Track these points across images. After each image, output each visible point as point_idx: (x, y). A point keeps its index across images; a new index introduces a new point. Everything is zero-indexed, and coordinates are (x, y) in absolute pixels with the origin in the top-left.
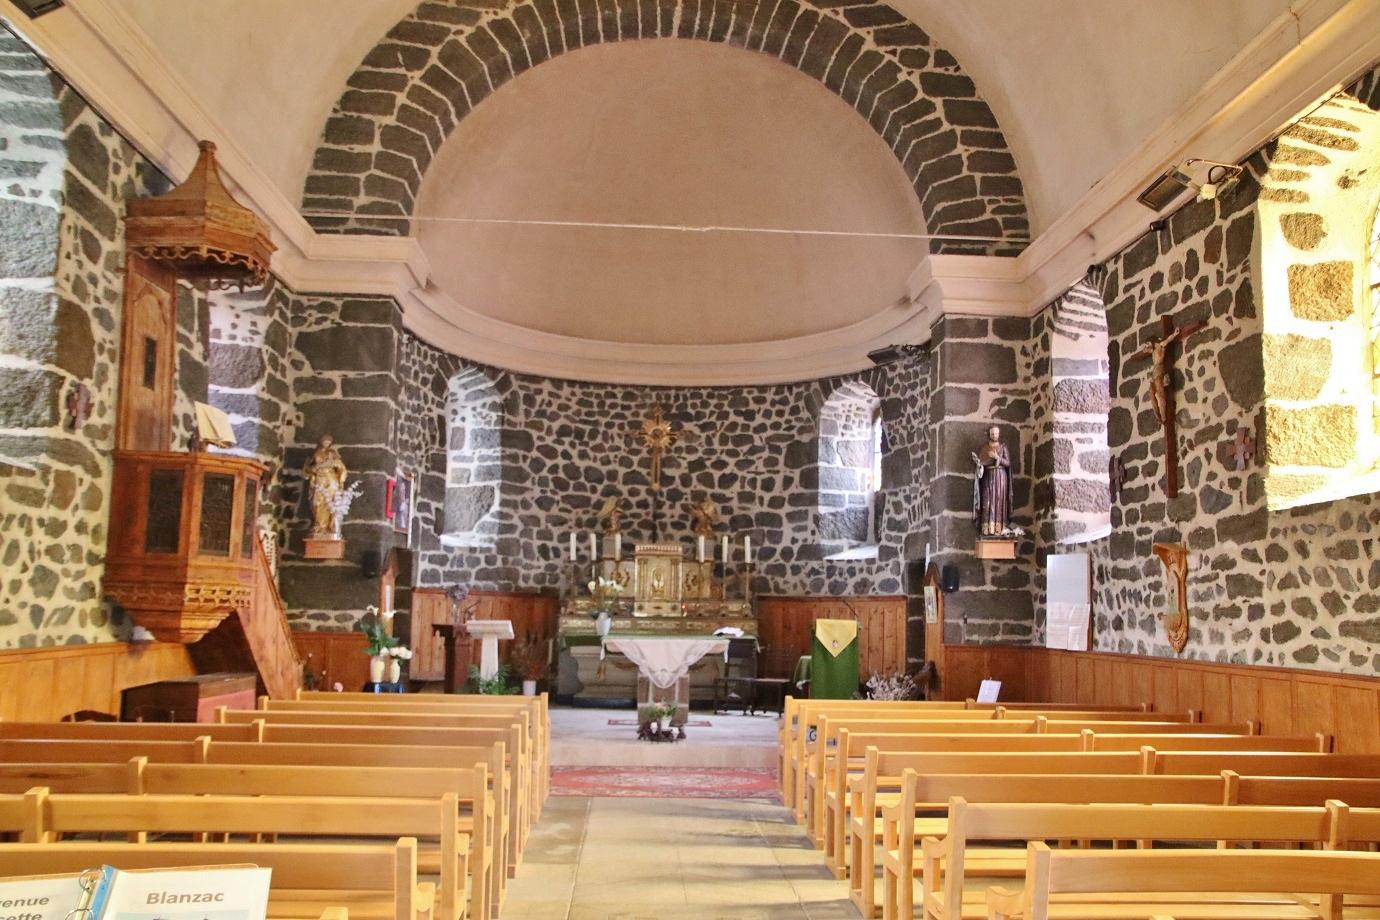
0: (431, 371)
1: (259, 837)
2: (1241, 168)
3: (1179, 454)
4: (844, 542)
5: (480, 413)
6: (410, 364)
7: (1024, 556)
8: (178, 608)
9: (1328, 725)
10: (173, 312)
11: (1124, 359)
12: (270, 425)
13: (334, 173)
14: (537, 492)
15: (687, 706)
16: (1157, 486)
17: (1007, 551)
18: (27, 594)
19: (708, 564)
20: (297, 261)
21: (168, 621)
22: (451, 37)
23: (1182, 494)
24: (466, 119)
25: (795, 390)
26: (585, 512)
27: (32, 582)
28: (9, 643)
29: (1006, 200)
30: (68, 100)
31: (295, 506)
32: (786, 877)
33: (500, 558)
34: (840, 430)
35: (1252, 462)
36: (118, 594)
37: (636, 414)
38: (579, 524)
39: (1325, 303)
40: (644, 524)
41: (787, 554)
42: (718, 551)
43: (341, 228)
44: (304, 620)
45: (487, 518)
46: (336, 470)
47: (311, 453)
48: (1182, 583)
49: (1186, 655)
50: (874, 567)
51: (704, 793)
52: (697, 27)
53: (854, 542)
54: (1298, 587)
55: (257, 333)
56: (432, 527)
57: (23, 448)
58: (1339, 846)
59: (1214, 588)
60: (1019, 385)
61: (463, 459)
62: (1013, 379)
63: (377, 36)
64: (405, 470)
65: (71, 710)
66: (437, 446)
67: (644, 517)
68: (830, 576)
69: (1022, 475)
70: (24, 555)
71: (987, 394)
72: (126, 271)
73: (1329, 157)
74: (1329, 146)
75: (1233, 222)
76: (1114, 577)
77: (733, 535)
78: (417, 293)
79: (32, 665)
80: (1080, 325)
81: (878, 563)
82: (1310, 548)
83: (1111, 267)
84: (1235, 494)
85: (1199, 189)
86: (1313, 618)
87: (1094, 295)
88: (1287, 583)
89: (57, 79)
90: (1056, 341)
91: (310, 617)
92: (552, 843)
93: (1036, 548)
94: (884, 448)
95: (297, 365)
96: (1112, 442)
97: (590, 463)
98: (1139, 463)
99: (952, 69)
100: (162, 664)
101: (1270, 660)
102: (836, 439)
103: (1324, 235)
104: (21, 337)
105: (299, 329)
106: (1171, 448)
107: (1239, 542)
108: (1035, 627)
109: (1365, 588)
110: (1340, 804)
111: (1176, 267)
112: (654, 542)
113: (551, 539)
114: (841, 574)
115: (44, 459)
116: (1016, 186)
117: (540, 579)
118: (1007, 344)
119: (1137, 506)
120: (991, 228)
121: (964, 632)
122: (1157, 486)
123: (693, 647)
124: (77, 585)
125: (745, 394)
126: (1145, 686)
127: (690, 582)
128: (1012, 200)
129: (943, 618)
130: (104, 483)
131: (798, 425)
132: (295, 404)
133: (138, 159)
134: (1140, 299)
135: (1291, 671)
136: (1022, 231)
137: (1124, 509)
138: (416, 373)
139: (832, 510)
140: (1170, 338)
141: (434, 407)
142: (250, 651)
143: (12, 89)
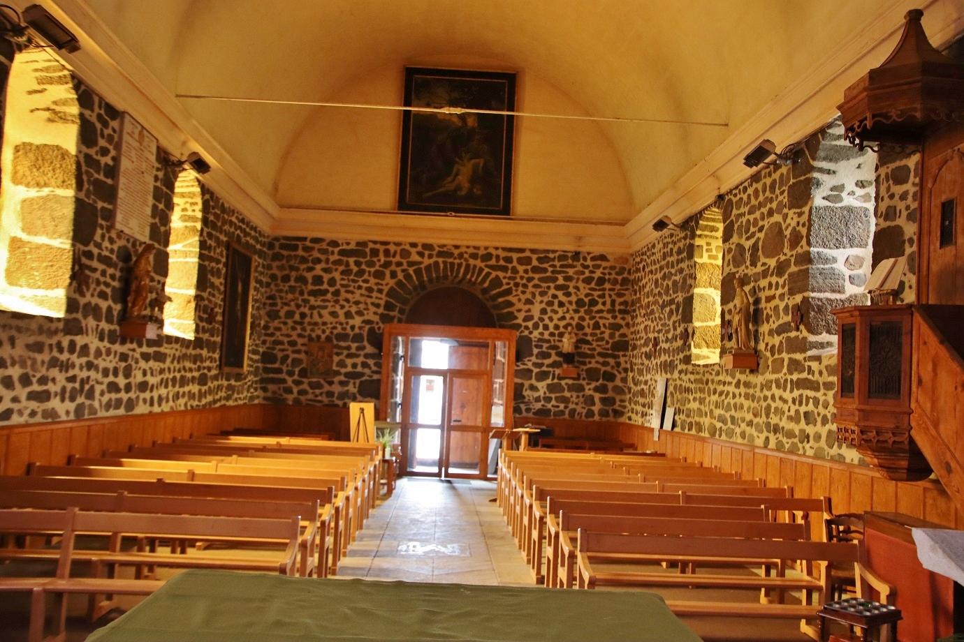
28: (852, 460)
82: (17, 342)
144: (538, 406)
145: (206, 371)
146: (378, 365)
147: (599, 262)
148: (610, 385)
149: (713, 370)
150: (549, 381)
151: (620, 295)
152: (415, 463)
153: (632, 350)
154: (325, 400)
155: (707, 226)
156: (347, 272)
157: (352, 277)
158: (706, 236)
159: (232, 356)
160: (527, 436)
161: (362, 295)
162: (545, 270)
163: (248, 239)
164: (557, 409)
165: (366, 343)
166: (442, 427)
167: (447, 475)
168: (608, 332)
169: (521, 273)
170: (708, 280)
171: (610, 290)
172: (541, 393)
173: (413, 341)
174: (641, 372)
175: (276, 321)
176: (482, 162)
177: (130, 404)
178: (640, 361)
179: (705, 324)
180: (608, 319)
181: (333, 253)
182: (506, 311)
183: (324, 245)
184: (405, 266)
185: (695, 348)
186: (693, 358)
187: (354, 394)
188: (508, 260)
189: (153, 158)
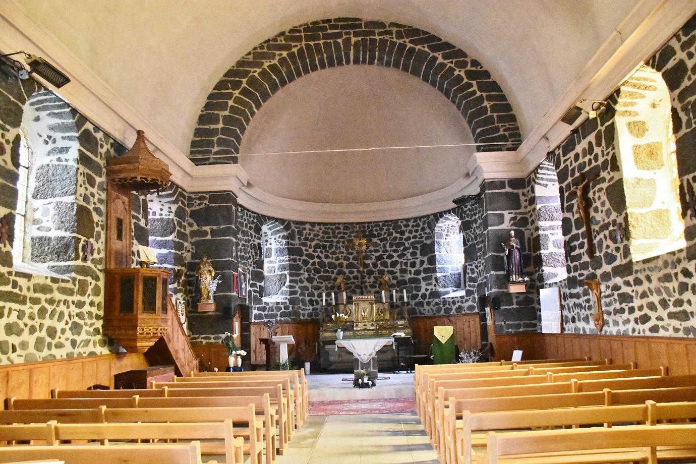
0: (253, 223)
1: (168, 440)
2: (606, 103)
3: (593, 237)
4: (450, 289)
5: (278, 241)
6: (243, 221)
7: (531, 290)
8: (135, 337)
9: (665, 362)
10: (129, 206)
11: (566, 194)
12: (180, 253)
13: (203, 138)
14: (306, 275)
15: (377, 370)
16: (585, 254)
17: (521, 289)
18: (68, 334)
19: (387, 304)
20: (188, 179)
21: (131, 344)
22: (251, 74)
23: (596, 256)
24: (261, 109)
25: (422, 220)
26: (329, 283)
27: (70, 329)
28: (61, 356)
29: (509, 125)
30: (79, 118)
31: (193, 289)
32: (409, 450)
33: (291, 306)
34: (445, 237)
35: (624, 239)
36: (110, 332)
37: (350, 236)
38: (327, 288)
39: (651, 162)
40: (357, 287)
41: (424, 296)
42: (391, 297)
43: (207, 162)
44: (200, 340)
45: (284, 288)
46: (210, 271)
47: (198, 264)
48: (599, 299)
49: (603, 333)
50: (464, 300)
51: (381, 412)
52: (361, 59)
53: (455, 289)
54: (648, 297)
55: (171, 212)
56: (258, 294)
57: (65, 271)
58: (653, 423)
59: (613, 300)
60: (522, 210)
61: (272, 262)
62: (519, 207)
63: (219, 76)
64: (243, 269)
65: (91, 385)
66: (258, 257)
67: (357, 283)
68: (444, 306)
69: (527, 252)
70: (66, 317)
71: (507, 215)
72: (107, 190)
73: (645, 95)
74: (644, 89)
75: (606, 127)
76: (570, 297)
77: (398, 289)
78: (244, 188)
79: (72, 366)
80: (547, 180)
81: (466, 298)
82: (652, 278)
83: (557, 152)
84: (618, 255)
85: (588, 113)
86: (656, 311)
87: (550, 165)
88: (644, 295)
89: (74, 111)
90: (537, 187)
91: (202, 338)
92: (305, 438)
93: (536, 284)
94: (465, 244)
95: (191, 225)
96: (564, 234)
97: (330, 260)
98: (576, 243)
99: (479, 67)
100: (132, 363)
101: (639, 333)
102: (442, 241)
103: (647, 130)
104: (62, 222)
105: (191, 209)
106: (589, 235)
107: (622, 277)
108: (538, 324)
109: (677, 296)
110: (652, 402)
111: (584, 150)
112: (362, 295)
113: (314, 296)
114: (449, 304)
115: (73, 275)
116: (513, 118)
117: (310, 315)
118: (515, 191)
119: (577, 263)
120: (503, 138)
121: (504, 328)
122: (585, 254)
123: (377, 343)
124: (91, 329)
125: (399, 223)
126: (587, 349)
127: (379, 312)
128: (512, 125)
129: (494, 322)
130: (101, 284)
131: (425, 236)
132: (191, 243)
133: (111, 141)
134: (571, 166)
135: (648, 338)
136: (518, 139)
137: (572, 265)
138: (246, 224)
139: (443, 274)
140: (584, 183)
141: (256, 239)
142: (171, 355)
143: (57, 118)
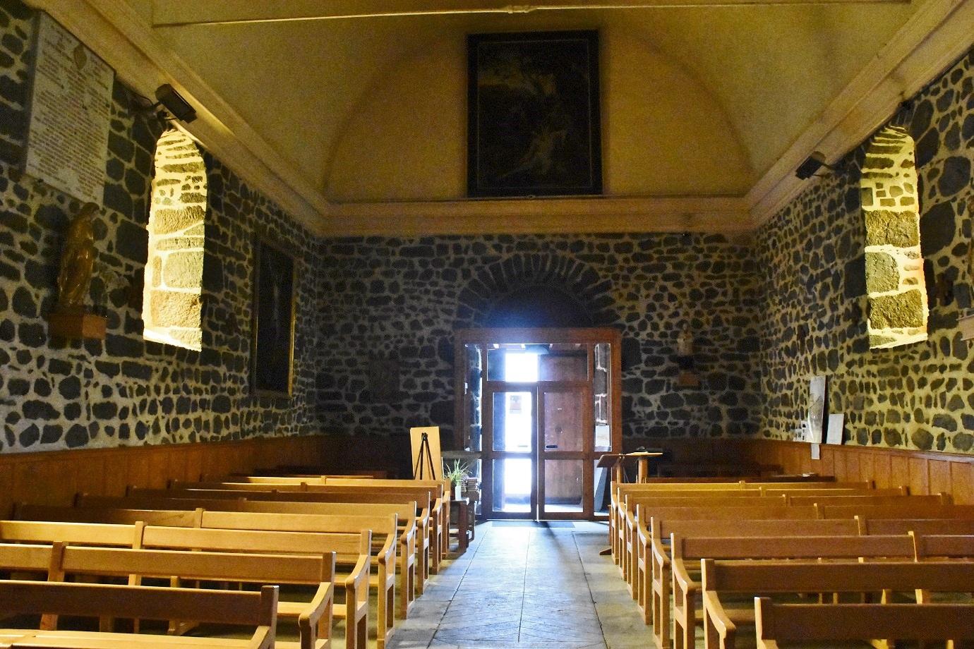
144: (652, 424)
145: (226, 394)
146: (452, 383)
147: (715, 244)
148: (739, 394)
149: (916, 352)
150: (663, 393)
151: (743, 282)
152: (503, 502)
153: (764, 349)
154: (391, 427)
155: (876, 159)
156: (411, 275)
157: (417, 280)
158: (875, 175)
159: (268, 377)
160: (646, 462)
161: (429, 301)
162: (649, 258)
163: (289, 237)
164: (675, 427)
165: (437, 357)
166: (533, 456)
167: (544, 515)
168: (732, 328)
169: (621, 263)
170: (884, 234)
171: (732, 276)
172: (654, 408)
173: (494, 353)
174: (781, 374)
175: (332, 337)
176: (563, 133)
177: (78, 436)
178: (778, 360)
179: (884, 294)
180: (732, 313)
181: (393, 253)
182: (604, 309)
183: (383, 245)
184: (480, 263)
185: (873, 327)
186: (871, 342)
187: (426, 419)
188: (604, 248)
189: (108, 95)
